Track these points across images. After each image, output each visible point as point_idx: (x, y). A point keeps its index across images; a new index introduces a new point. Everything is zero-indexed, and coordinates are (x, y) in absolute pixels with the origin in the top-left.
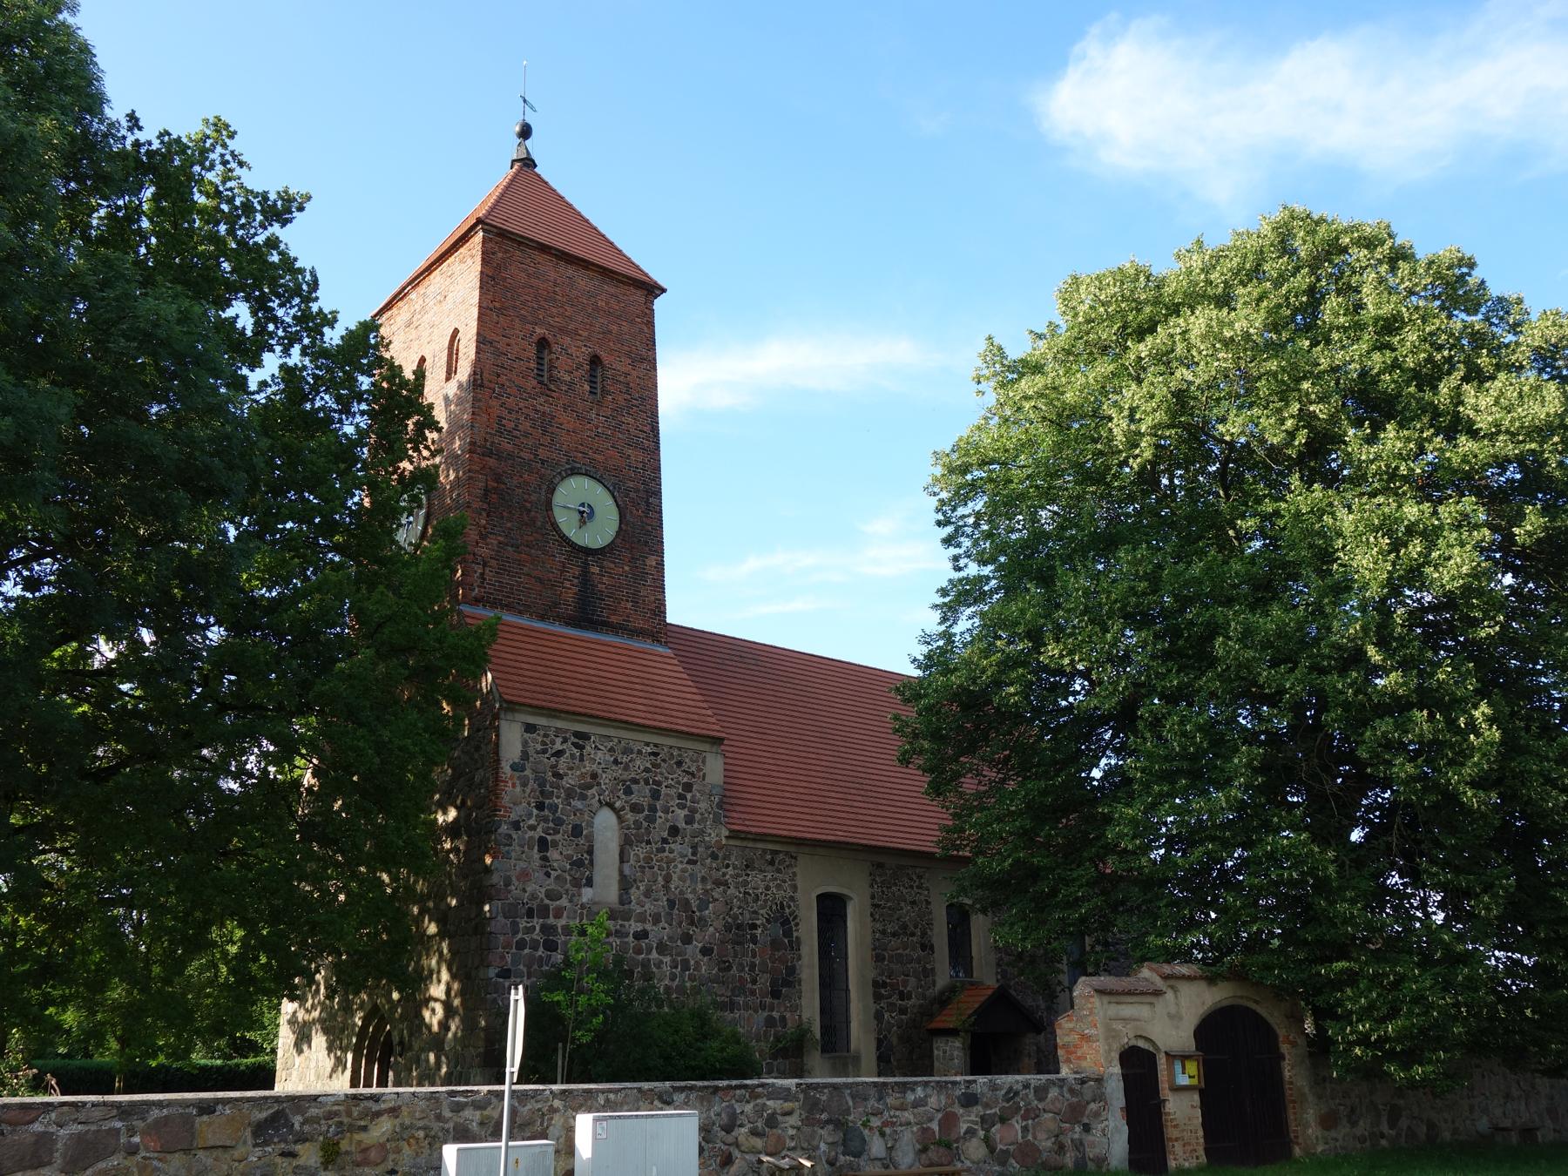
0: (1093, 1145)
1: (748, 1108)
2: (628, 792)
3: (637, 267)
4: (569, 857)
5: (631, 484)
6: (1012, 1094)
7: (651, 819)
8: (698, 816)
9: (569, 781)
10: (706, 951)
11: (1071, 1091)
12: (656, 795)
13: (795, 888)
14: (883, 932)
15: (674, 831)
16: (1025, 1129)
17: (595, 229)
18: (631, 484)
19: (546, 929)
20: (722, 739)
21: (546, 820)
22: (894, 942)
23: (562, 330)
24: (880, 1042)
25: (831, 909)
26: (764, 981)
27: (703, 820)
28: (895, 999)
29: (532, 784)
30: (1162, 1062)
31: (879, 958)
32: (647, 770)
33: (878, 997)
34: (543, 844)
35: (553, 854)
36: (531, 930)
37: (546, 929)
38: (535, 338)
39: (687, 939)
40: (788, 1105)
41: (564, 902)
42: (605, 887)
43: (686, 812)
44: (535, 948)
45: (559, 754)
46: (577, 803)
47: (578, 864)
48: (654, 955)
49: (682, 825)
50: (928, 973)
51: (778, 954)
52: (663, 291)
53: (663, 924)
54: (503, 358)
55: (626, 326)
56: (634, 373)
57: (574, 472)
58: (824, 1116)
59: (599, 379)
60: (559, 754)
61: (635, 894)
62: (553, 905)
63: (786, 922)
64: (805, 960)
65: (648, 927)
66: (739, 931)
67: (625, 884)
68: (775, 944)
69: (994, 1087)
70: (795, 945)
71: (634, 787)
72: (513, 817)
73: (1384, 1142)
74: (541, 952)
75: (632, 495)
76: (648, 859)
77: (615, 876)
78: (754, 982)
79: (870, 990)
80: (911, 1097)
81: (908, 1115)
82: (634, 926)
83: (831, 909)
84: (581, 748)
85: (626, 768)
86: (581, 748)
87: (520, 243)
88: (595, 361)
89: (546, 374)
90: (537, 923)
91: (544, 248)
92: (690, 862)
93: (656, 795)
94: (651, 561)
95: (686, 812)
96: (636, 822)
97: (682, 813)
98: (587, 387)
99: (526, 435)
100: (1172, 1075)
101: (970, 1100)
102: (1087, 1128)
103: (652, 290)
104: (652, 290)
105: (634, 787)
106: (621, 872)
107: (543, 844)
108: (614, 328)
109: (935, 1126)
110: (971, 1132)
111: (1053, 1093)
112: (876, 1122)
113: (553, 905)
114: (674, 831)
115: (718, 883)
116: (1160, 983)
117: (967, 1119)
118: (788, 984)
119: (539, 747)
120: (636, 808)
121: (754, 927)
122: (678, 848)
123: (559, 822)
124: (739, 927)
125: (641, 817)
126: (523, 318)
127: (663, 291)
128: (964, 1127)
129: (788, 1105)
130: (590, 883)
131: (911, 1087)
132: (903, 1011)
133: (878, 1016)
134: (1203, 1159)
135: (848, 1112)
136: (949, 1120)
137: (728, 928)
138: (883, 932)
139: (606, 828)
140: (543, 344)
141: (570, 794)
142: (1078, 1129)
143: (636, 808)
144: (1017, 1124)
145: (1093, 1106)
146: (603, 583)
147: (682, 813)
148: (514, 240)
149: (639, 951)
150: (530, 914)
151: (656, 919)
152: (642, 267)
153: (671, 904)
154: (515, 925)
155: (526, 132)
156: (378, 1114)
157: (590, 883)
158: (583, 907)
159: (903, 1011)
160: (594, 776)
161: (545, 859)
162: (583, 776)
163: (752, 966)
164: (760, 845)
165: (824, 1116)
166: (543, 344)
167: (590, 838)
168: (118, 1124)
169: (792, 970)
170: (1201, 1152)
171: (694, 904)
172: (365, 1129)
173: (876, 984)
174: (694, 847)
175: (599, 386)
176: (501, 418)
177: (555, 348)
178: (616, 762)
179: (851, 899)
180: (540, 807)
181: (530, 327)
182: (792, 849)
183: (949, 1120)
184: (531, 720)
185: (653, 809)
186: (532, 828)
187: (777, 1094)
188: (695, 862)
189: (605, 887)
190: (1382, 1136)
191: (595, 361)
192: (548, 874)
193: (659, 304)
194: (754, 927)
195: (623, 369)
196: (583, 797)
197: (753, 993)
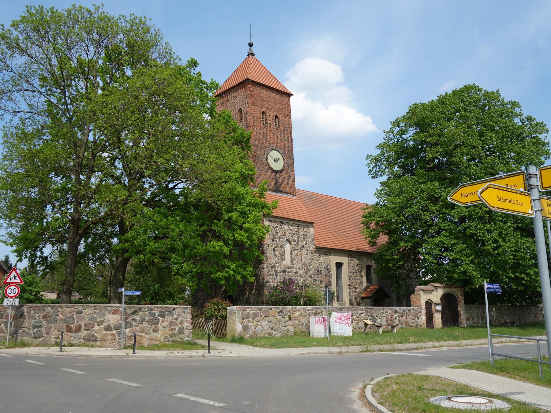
0: (419, 322)
1: (356, 312)
2: (292, 237)
3: (285, 88)
4: (280, 253)
5: (286, 152)
6: (404, 311)
7: (298, 244)
8: (308, 243)
9: (280, 234)
10: (310, 277)
11: (415, 310)
12: (298, 238)
13: (330, 261)
14: (351, 272)
15: (303, 246)
16: (406, 318)
17: (265, 68)
18: (286, 152)
19: (276, 271)
20: (313, 223)
21: (274, 244)
22: (353, 275)
23: (268, 109)
24: (350, 300)
25: (339, 265)
26: (324, 284)
27: (309, 244)
28: (353, 289)
29: (271, 236)
30: (433, 305)
31: (350, 279)
32: (296, 231)
33: (350, 289)
34: (274, 250)
35: (276, 252)
36: (272, 271)
37: (276, 271)
38: (262, 112)
39: (306, 274)
40: (363, 312)
41: (279, 264)
42: (287, 262)
43: (305, 242)
44: (273, 276)
45: (277, 227)
46: (281, 240)
47: (282, 255)
48: (299, 277)
49: (304, 245)
50: (361, 282)
51: (327, 277)
52: (293, 95)
53: (301, 270)
54: (255, 118)
55: (283, 107)
56: (286, 120)
57: (273, 150)
58: (369, 314)
59: (277, 122)
60: (277, 227)
61: (295, 262)
62: (277, 265)
63: (328, 269)
64: (333, 279)
65: (298, 271)
66: (318, 272)
67: (292, 261)
68: (326, 275)
69: (400, 309)
70: (330, 275)
71: (294, 235)
72: (268, 243)
73: (480, 324)
74: (274, 277)
75: (287, 155)
76: (297, 254)
77: (290, 258)
78: (321, 284)
79: (348, 287)
80: (385, 311)
81: (384, 315)
82: (294, 270)
83: (339, 265)
84: (282, 226)
85: (292, 231)
86: (282, 226)
87: (257, 84)
88: (276, 117)
89: (264, 121)
90: (274, 269)
91: (263, 85)
92: (307, 254)
93: (298, 238)
94: (291, 173)
95: (305, 242)
96: (294, 244)
97: (305, 242)
98: (275, 125)
99: (261, 139)
100: (435, 308)
101: (396, 312)
102: (418, 319)
103: (289, 95)
104: (289, 95)
105: (294, 235)
106: (291, 257)
107: (274, 250)
108: (281, 107)
109: (389, 317)
110: (396, 318)
111: (412, 311)
112: (378, 316)
113: (277, 265)
114: (303, 246)
115: (313, 260)
116: (433, 288)
117: (395, 316)
118: (329, 285)
119: (273, 226)
120: (294, 241)
121: (321, 271)
122: (304, 250)
123: (277, 245)
124: (318, 271)
125: (295, 243)
126: (259, 106)
127: (293, 95)
128: (395, 317)
129: (363, 312)
130: (284, 260)
131: (385, 309)
132: (355, 292)
133: (350, 293)
134: (441, 326)
135: (373, 313)
136: (392, 316)
137: (315, 271)
138: (351, 272)
139: (288, 247)
140: (264, 113)
141: (280, 238)
142: (416, 318)
143: (294, 241)
144: (404, 317)
145: (420, 314)
146: (280, 180)
147: (305, 242)
148: (255, 83)
149: (296, 277)
150: (272, 267)
151: (299, 269)
152: (287, 88)
153: (303, 265)
154: (269, 270)
155: (251, 45)
156: (296, 311)
157: (284, 260)
158: (283, 266)
159: (355, 292)
160: (285, 233)
161: (275, 254)
162: (282, 233)
163: (321, 280)
164: (322, 250)
165: (369, 314)
166: (264, 113)
167: (284, 248)
168: (258, 311)
169: (330, 282)
170: (441, 324)
171: (308, 265)
172: (295, 313)
173: (349, 285)
174: (307, 250)
175: (277, 124)
176: (255, 135)
177: (267, 114)
178: (289, 229)
179: (343, 264)
180: (273, 241)
181: (260, 108)
182: (330, 251)
183: (392, 316)
184: (271, 219)
185: (298, 241)
186: (272, 246)
187: (362, 310)
188: (307, 254)
189: (287, 262)
190: (480, 323)
191: (276, 117)
192: (275, 258)
193: (291, 98)
194: (321, 271)
195: (283, 119)
196: (283, 238)
197: (321, 287)
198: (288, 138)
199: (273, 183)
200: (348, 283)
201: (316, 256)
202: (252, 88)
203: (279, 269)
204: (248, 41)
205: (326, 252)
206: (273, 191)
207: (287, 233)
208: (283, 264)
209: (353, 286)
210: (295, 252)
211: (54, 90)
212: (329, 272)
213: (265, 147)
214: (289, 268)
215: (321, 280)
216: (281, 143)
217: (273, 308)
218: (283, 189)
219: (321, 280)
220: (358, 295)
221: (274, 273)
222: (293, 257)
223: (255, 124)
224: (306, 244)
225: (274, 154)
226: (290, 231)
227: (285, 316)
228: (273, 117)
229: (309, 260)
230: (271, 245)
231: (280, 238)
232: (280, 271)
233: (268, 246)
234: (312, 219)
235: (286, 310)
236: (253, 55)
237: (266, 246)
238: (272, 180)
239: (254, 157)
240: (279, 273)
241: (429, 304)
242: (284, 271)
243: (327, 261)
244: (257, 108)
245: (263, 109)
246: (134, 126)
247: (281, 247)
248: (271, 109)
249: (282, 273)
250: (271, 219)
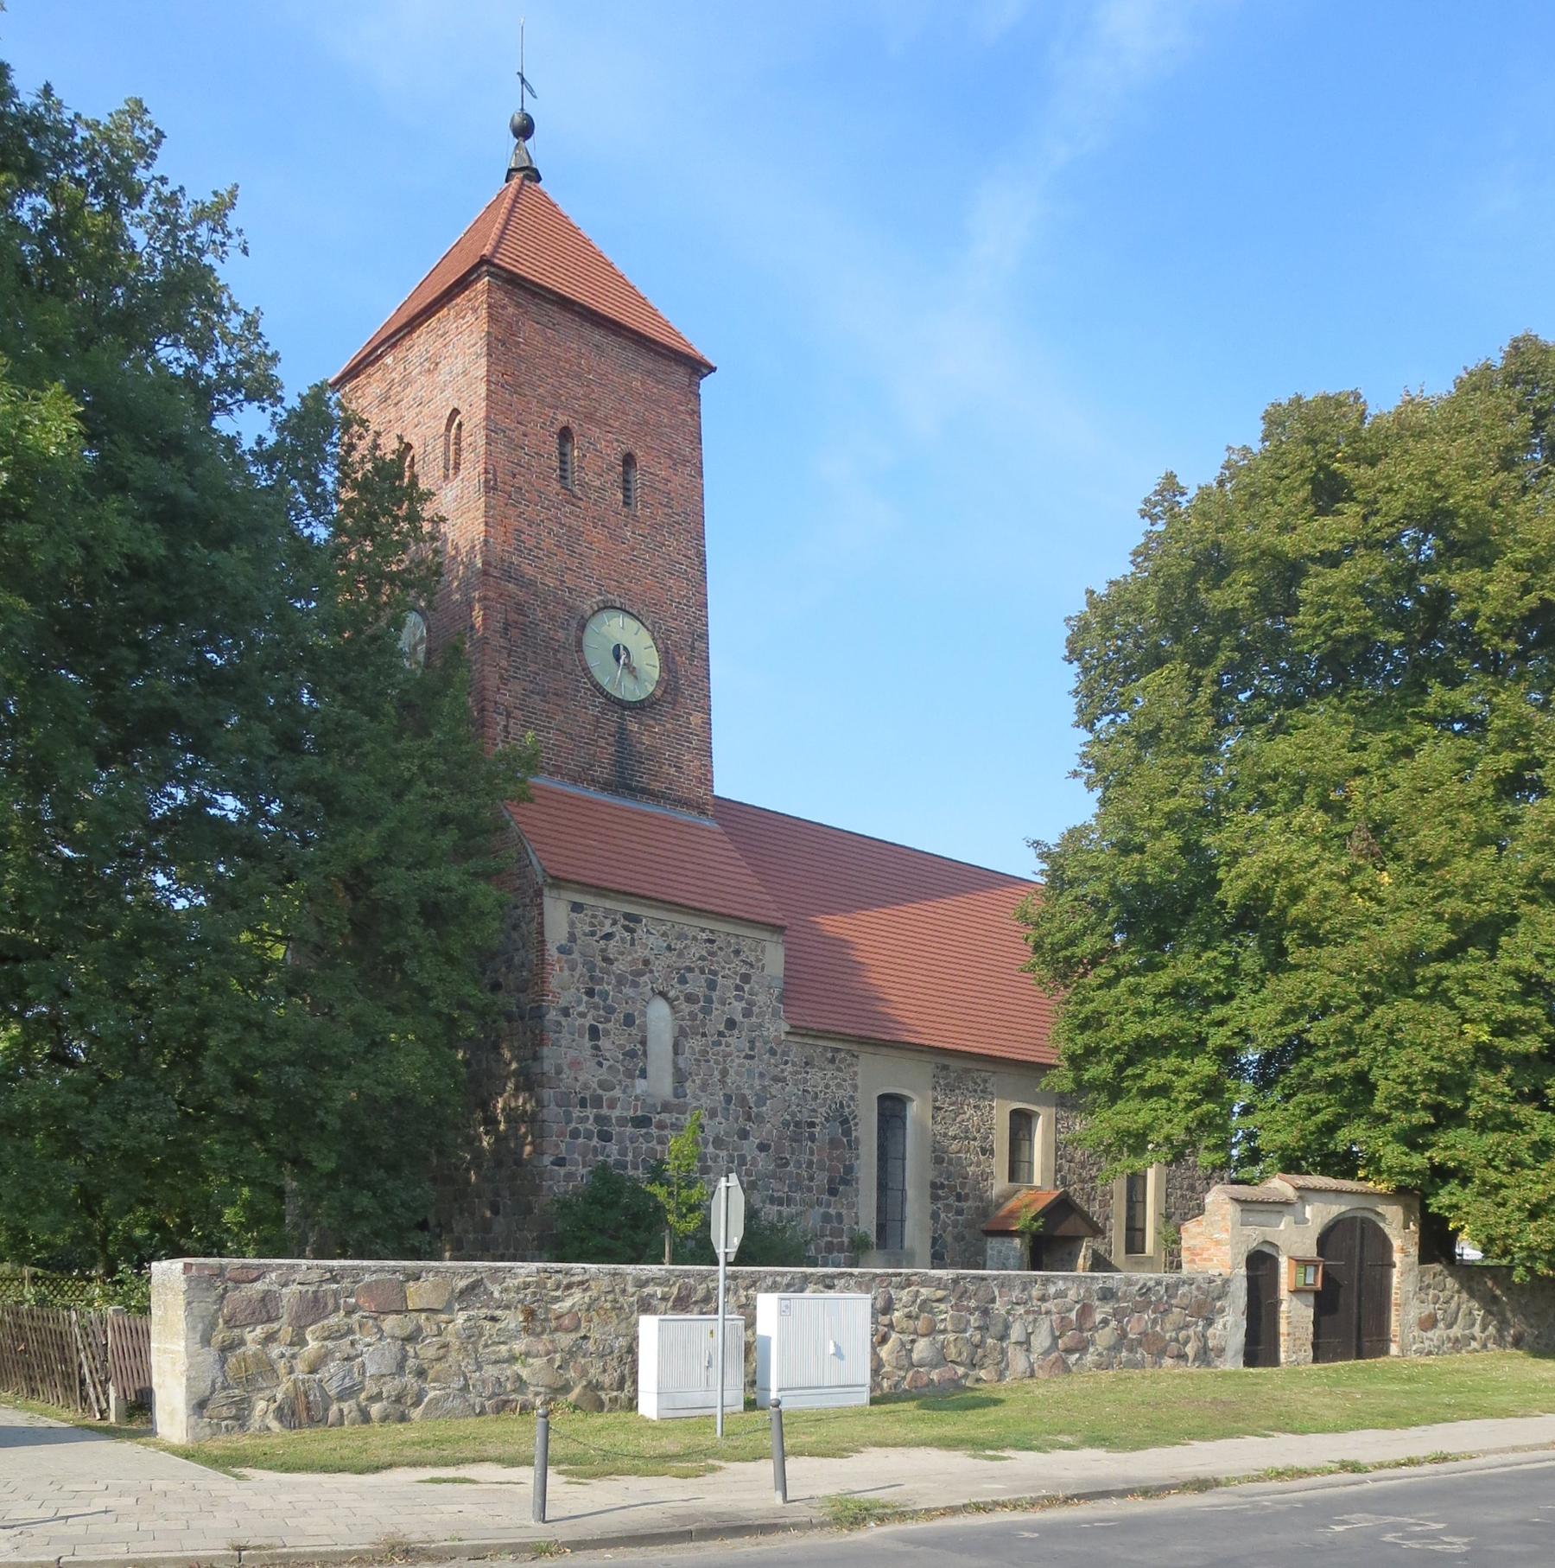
2: (683, 981)
3: (678, 335)
4: (621, 1047)
7: (707, 1011)
8: (755, 1009)
9: (619, 967)
10: (763, 1147)
12: (712, 985)
13: (855, 1087)
15: (731, 1024)
23: (590, 417)
24: (935, 1241)
26: (822, 1178)
28: (951, 1200)
33: (935, 1198)
34: (594, 1033)
35: (604, 1043)
36: (584, 1119)
39: (744, 1135)
41: (617, 1093)
44: (589, 1137)
46: (628, 990)
47: (632, 1054)
48: (711, 1149)
49: (739, 1018)
51: (836, 1153)
52: (713, 369)
58: (973, 1304)
62: (606, 1095)
63: (845, 1121)
66: (800, 1129)
67: (680, 1077)
68: (834, 1143)
70: (853, 1145)
72: (563, 1003)
74: (595, 1142)
77: (670, 1069)
78: (811, 1179)
79: (928, 1191)
80: (1052, 1290)
84: (632, 931)
85: (680, 955)
87: (535, 295)
90: (590, 1112)
92: (748, 1057)
93: (712, 985)
94: (696, 719)
95: (743, 1004)
96: (690, 1013)
104: (698, 368)
106: (675, 1064)
109: (1073, 1316)
113: (606, 1095)
114: (731, 1024)
115: (776, 1079)
120: (691, 999)
121: (812, 1125)
122: (735, 1042)
123: (610, 1010)
124: (797, 1124)
127: (713, 369)
130: (643, 1074)
132: (959, 1212)
133: (935, 1216)
136: (1086, 1311)
140: (565, 434)
141: (621, 981)
143: (691, 999)
150: (583, 1103)
151: (713, 1114)
153: (728, 1099)
155: (524, 130)
156: (569, 1286)
157: (643, 1074)
158: (637, 1098)
159: (959, 1212)
160: (646, 962)
161: (597, 1048)
167: (643, 1028)
169: (849, 1169)
171: (752, 1101)
173: (934, 1186)
178: (669, 948)
180: (590, 993)
182: (854, 1047)
183: (1086, 1311)
184: (578, 898)
185: (709, 1000)
186: (582, 1015)
188: (751, 1057)
189: (659, 1082)
192: (600, 1064)
197: (810, 1189)
198: (686, 561)
199: (606, 751)
200: (930, 1176)
201: (789, 1068)
202: (510, 310)
203: (616, 1113)
204: (509, 113)
205: (837, 1050)
206: (606, 787)
207: (658, 966)
208: (638, 1092)
209: (952, 1188)
210: (694, 1044)
211: (1509, 1315)
212: (847, 1133)
213: (570, 590)
214: (666, 1108)
215: (810, 1164)
216: (650, 581)
217: (429, 1270)
218: (655, 786)
219: (810, 1164)
220: (969, 1225)
221: (590, 1125)
222: (682, 1065)
223: (519, 481)
224: (747, 1013)
225: (617, 629)
226: (672, 958)
227: (498, 1313)
228: (615, 458)
229: (757, 1082)
230: (582, 1008)
231: (621, 981)
232: (622, 1121)
233: (566, 1012)
234: (779, 915)
235: (510, 1283)
236: (533, 175)
237: (552, 1015)
238: (602, 743)
239: (513, 632)
240: (615, 1130)
241: (1261, 1264)
242: (642, 1122)
243: (839, 1086)
244: (534, 406)
245: (563, 419)
246: (1185, 1144)
247: (629, 1020)
248: (603, 423)
249: (629, 1130)
250: (578, 898)
